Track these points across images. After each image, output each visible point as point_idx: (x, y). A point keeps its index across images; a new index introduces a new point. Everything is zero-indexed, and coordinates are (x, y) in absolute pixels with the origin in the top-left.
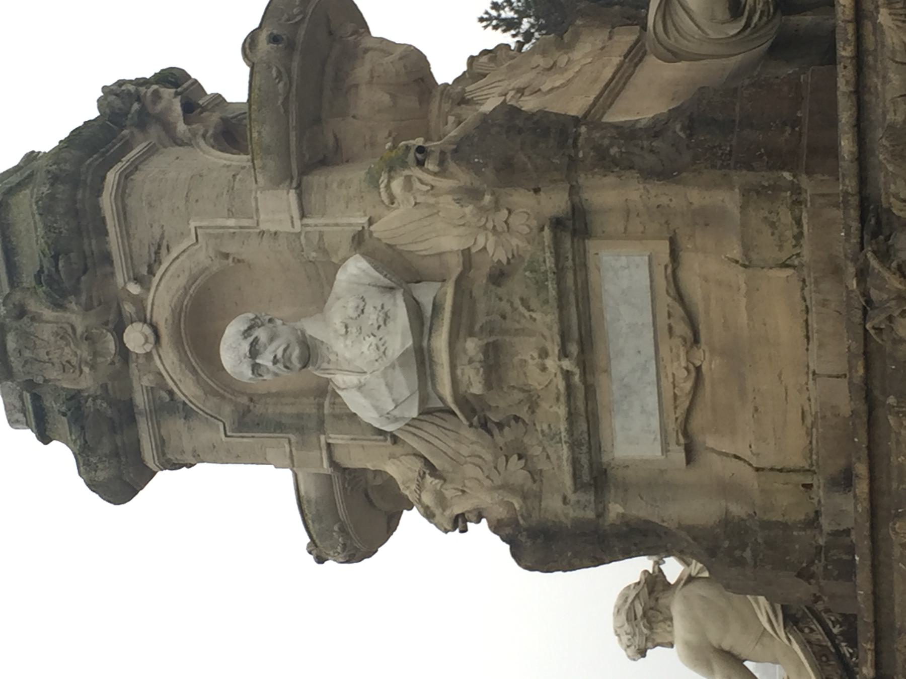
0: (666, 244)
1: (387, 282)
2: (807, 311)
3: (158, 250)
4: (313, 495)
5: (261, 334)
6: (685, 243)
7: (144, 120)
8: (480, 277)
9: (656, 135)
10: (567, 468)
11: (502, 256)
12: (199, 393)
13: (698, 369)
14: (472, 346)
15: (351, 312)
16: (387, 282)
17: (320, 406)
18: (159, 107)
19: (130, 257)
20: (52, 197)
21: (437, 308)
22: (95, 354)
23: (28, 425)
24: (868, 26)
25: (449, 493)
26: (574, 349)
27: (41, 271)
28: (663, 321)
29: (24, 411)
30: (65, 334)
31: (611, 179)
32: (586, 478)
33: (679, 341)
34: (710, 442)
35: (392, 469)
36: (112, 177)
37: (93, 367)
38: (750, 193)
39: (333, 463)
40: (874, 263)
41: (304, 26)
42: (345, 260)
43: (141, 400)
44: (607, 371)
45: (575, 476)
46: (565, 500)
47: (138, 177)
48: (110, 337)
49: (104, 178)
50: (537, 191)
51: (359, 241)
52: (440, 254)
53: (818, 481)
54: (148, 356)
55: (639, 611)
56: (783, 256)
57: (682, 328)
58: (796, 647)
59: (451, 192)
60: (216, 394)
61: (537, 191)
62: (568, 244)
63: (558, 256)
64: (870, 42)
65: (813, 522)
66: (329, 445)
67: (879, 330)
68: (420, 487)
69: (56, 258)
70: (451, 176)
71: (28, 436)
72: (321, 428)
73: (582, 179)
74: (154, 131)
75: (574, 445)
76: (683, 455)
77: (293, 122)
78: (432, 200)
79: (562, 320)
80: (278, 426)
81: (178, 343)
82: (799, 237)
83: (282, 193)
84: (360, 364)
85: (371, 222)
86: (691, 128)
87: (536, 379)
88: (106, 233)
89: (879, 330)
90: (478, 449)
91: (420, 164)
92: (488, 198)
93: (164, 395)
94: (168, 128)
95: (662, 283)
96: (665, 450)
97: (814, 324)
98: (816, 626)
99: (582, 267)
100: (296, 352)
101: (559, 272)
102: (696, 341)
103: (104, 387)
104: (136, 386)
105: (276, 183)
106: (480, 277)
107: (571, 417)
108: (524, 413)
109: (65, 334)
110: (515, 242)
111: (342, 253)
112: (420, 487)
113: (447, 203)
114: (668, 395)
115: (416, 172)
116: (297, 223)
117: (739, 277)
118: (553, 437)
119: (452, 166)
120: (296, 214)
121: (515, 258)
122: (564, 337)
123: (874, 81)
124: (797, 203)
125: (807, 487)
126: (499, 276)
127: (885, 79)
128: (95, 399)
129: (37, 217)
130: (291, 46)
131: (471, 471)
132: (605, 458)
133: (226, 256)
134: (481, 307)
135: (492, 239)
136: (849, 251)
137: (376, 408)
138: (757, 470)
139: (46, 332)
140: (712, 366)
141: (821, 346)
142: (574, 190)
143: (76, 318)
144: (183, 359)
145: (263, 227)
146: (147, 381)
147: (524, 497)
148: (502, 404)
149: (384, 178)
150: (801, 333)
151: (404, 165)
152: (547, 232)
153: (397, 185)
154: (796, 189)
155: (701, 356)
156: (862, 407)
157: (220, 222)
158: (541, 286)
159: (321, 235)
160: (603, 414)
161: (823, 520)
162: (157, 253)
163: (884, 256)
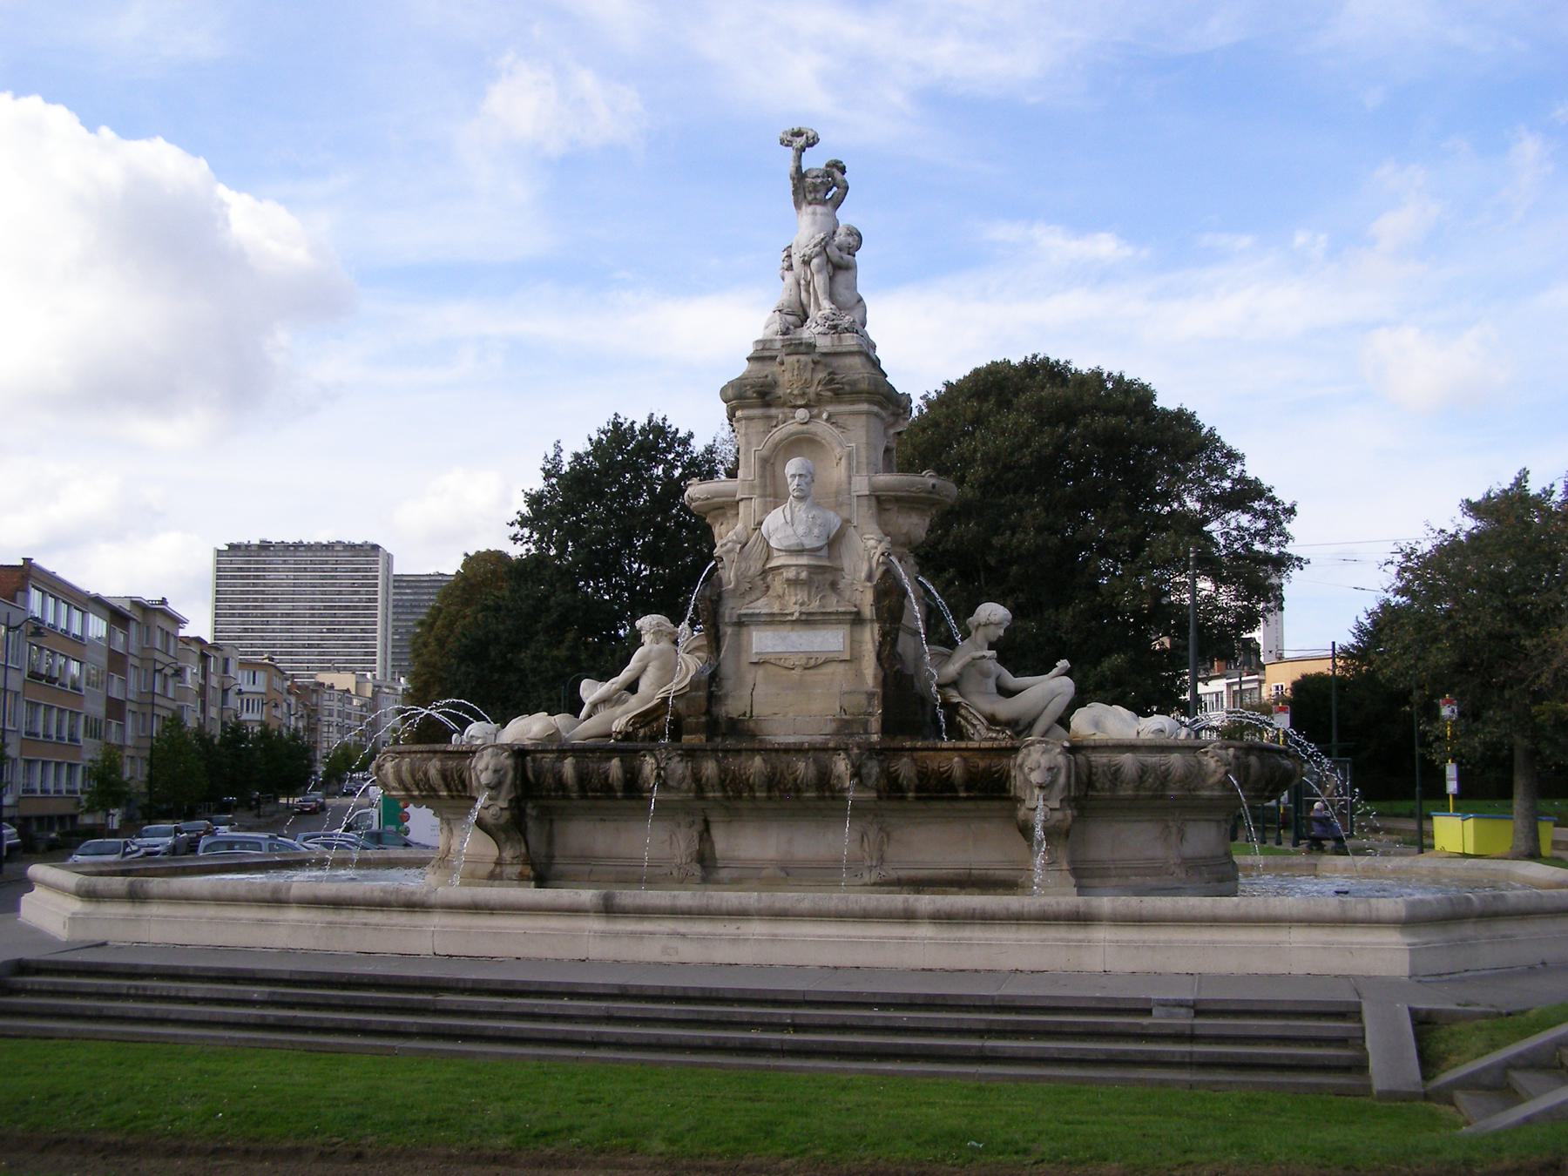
0: (848, 658)
1: (831, 536)
7: (896, 415)
13: (793, 669)
17: (770, 496)
18: (901, 421)
26: (804, 617)
32: (743, 619)
39: (742, 500)
43: (773, 411)
44: (792, 630)
45: (745, 615)
48: (803, 403)
54: (794, 418)
57: (812, 662)
62: (848, 617)
63: (844, 613)
70: (877, 568)
74: (891, 419)
77: (900, 494)
94: (892, 425)
95: (831, 656)
96: (756, 653)
99: (839, 622)
102: (805, 669)
107: (772, 615)
112: (733, 541)
116: (855, 494)
120: (858, 494)
132: (752, 627)
134: (820, 577)
136: (93, 672)
147: (734, 590)
152: (855, 609)
160: (773, 627)
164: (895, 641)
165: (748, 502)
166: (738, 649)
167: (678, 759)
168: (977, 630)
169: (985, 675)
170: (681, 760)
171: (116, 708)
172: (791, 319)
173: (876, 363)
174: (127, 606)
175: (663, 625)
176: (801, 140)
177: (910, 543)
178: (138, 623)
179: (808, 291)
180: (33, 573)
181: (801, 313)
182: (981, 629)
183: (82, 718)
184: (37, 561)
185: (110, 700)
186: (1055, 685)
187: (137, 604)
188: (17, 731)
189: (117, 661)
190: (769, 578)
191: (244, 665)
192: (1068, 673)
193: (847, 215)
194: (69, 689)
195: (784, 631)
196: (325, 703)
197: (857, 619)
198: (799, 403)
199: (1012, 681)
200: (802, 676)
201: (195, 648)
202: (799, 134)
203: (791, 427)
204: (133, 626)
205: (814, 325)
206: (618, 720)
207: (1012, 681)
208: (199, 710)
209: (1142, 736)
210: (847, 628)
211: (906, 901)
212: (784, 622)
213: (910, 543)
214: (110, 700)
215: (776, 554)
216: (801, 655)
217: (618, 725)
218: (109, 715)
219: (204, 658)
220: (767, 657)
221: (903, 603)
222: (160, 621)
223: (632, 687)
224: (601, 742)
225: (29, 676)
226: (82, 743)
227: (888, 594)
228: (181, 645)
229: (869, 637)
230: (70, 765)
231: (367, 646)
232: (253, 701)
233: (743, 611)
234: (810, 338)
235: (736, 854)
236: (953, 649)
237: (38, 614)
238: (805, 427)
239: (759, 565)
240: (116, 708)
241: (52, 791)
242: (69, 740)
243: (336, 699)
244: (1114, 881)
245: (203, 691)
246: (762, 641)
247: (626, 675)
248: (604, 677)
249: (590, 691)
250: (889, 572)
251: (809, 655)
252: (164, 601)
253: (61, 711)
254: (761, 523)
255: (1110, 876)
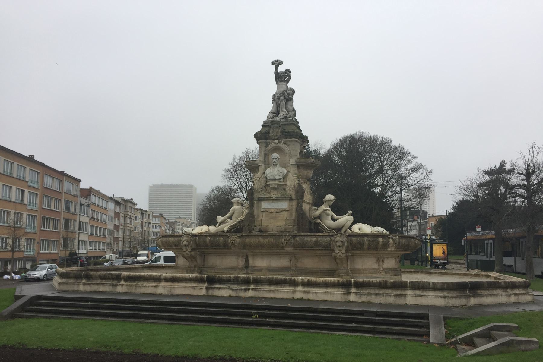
1: (284, 175)
2: (281, 226)
3: (288, 145)
4: (255, 162)
5: (278, 159)
6: (288, 212)
7: (303, 142)
8: (284, 187)
9: (301, 209)
10: (261, 197)
11: (287, 190)
12: (269, 149)
14: (276, 186)
15: (281, 171)
16: (284, 175)
17: (267, 164)
18: (305, 143)
19: (287, 141)
20: (295, 133)
21: (281, 182)
22: (274, 136)
23: (264, 124)
24: (315, 237)
25: (257, 181)
26: (276, 198)
27: (285, 130)
28: (279, 209)
29: (266, 123)
30: (277, 133)
31: (296, 204)
33: (276, 211)
34: (264, 214)
35: (259, 173)
36: (297, 140)
37: (273, 136)
38: (294, 221)
39: (260, 165)
40: (290, 237)
41: (314, 165)
42: (286, 170)
43: (268, 141)
44: (273, 202)
45: (260, 198)
46: (256, 196)
47: (297, 143)
49: (297, 138)
50: (295, 195)
51: (288, 172)
52: (287, 181)
53: (260, 227)
54: (274, 143)
55: (239, 202)
56: (287, 224)
57: (278, 211)
58: (236, 222)
59: (295, 184)
60: (269, 151)
61: (295, 195)
64: (313, 237)
65: (255, 226)
66: (262, 165)
67: (283, 237)
68: (257, 177)
69: (287, 133)
70: (296, 184)
71: (262, 124)
72: (265, 164)
73: (296, 200)
74: (302, 143)
75: (264, 198)
76: (262, 211)
77: (303, 164)
78: (294, 181)
79: (279, 197)
80: (265, 159)
81: (275, 147)
82: (289, 226)
83: (295, 162)
84: (274, 172)
85: (291, 173)
86: (302, 214)
87: (272, 193)
88: (290, 138)
89: (283, 237)
90: (262, 185)
91: (298, 181)
92: (294, 189)
93: (269, 144)
94: (302, 145)
96: (263, 209)
97: (279, 227)
98: (239, 224)
99: (286, 200)
100: (275, 164)
101: (285, 197)
103: (270, 137)
104: (270, 140)
105: (296, 161)
106: (284, 187)
107: (267, 198)
108: (267, 191)
109: (277, 133)
110: (289, 191)
111: (287, 169)
112: (257, 177)
113: (293, 184)
114: (269, 209)
115: (297, 180)
117: (285, 219)
118: (265, 195)
119: (298, 184)
121: (286, 191)
122: (277, 197)
123: (309, 237)
124: (293, 226)
125: (259, 226)
126: (284, 189)
127: (309, 238)
128: (269, 135)
129: (292, 130)
130: (312, 163)
131: (260, 184)
133: (287, 154)
134: (281, 187)
135: (289, 189)
137: (268, 173)
138: (261, 220)
139: (277, 130)
140: (274, 215)
141: (277, 228)
142: (295, 199)
143: (279, 134)
144: (273, 147)
145: (290, 159)
146: (271, 142)
147: (257, 191)
148: (268, 189)
149: (296, 176)
150: (278, 225)
151: (298, 179)
152: (290, 196)
153: (296, 177)
154: (295, 226)
155: (275, 213)
156: (274, 235)
157: (291, 154)
158: (283, 195)
159: (289, 167)
161: (255, 227)
162: (287, 145)
163: (291, 238)
164: (301, 206)
165: (261, 166)
166: (259, 207)
167: (238, 238)
168: (325, 202)
169: (328, 215)
170: (239, 238)
171: (116, 227)
172: (275, 115)
173: (298, 127)
174: (120, 200)
175: (239, 201)
176: (277, 63)
177: (307, 178)
178: (123, 205)
179: (279, 107)
180: (92, 191)
181: (277, 113)
182: (327, 202)
183: (107, 230)
184: (93, 187)
185: (115, 225)
186: (346, 219)
187: (123, 200)
188: (88, 233)
189: (117, 215)
190: (267, 187)
191: (154, 216)
192: (352, 215)
193: (290, 85)
194: (103, 222)
195: (271, 202)
196: (177, 226)
197: (290, 199)
198: (275, 138)
199: (336, 216)
200: (275, 215)
201: (140, 212)
202: (277, 61)
203: (272, 145)
204: (122, 206)
205: (280, 116)
206: (226, 227)
207: (336, 216)
208: (141, 228)
209: (372, 233)
210: (288, 201)
211: (302, 279)
212: (270, 200)
213: (307, 178)
214: (115, 225)
215: (268, 181)
216: (275, 209)
217: (226, 229)
218: (115, 229)
219: (142, 214)
220: (266, 210)
221: (303, 194)
222: (129, 204)
223: (230, 218)
224: (221, 233)
225: (91, 218)
226: (106, 237)
227: (300, 193)
228: (135, 211)
229: (294, 203)
230: (103, 243)
231: (189, 212)
232: (155, 226)
233: (259, 197)
234: (279, 120)
235: (255, 265)
236: (319, 208)
237: (94, 202)
238: (277, 145)
239: (264, 184)
240: (116, 227)
241: (98, 250)
242: (103, 236)
243: (180, 225)
244: (363, 275)
245: (142, 223)
246: (265, 205)
247: (228, 215)
248: (223, 216)
249: (220, 219)
250: (300, 186)
251: (277, 209)
252: (132, 199)
253: (100, 228)
254: (264, 172)
255: (361, 273)
